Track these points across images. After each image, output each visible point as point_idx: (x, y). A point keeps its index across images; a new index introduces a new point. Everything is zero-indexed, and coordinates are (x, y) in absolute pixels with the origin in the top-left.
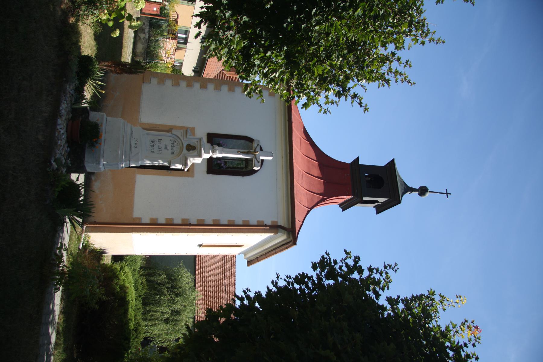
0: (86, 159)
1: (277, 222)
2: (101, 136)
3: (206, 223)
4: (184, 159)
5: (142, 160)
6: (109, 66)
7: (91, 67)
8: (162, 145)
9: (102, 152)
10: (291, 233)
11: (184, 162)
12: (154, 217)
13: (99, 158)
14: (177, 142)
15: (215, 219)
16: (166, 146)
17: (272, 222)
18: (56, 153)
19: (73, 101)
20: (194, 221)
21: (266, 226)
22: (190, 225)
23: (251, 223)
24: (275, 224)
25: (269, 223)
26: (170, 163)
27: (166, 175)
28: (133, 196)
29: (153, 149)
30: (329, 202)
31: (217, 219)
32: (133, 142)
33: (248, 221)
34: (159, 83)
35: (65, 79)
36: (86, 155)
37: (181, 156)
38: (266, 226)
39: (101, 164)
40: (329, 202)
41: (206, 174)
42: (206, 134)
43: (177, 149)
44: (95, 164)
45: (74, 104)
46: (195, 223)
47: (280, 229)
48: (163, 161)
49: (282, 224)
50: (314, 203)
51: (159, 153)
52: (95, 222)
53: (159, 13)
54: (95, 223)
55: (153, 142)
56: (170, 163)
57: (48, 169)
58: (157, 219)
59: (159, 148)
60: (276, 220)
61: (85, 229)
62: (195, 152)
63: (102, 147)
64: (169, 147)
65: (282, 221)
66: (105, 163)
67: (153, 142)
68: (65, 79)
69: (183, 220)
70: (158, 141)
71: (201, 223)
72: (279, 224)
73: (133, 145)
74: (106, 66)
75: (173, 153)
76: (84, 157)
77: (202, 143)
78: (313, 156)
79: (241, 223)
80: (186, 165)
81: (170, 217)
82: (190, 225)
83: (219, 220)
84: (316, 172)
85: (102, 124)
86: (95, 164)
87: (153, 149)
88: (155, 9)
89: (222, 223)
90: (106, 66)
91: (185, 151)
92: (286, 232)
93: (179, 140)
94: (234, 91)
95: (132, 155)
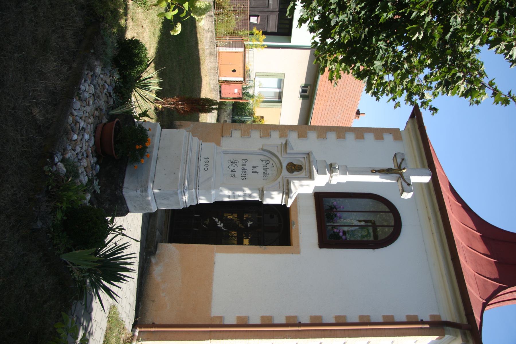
0: (126, 185)
1: (439, 316)
2: (151, 152)
3: (325, 321)
4: (285, 183)
5: (217, 188)
6: (174, 104)
7: (137, 51)
8: (249, 167)
9: (151, 174)
10: (468, 332)
11: (285, 188)
12: (243, 314)
13: (147, 182)
14: (271, 162)
15: (338, 314)
16: (254, 170)
17: (431, 316)
18: (65, 150)
19: (111, 103)
20: (305, 320)
21: (422, 322)
22: (300, 325)
23: (397, 319)
24: (436, 319)
25: (427, 319)
26: (262, 195)
27: (259, 253)
28: (211, 284)
29: (233, 174)
30: (508, 297)
31: (342, 314)
32: (202, 163)
33: (392, 317)
34: (242, 136)
35: (92, 51)
36: (126, 180)
37: (280, 179)
38: (422, 322)
39: (150, 191)
40: (508, 297)
41: (319, 249)
42: (315, 179)
43: (272, 172)
44: (139, 192)
45: (113, 108)
46: (308, 321)
47: (448, 328)
48: (250, 189)
49: (449, 319)
50: (490, 294)
51: (244, 178)
52: (153, 323)
53: (240, 96)
54: (153, 325)
55: (234, 163)
56: (262, 195)
57: (46, 168)
58: (247, 318)
59: (244, 170)
60: (436, 313)
61: (137, 334)
62: (303, 173)
63: (152, 168)
64: (260, 170)
65: (448, 314)
66: (156, 191)
67: (234, 163)
68: (92, 51)
69: (288, 318)
70: (241, 161)
71: (317, 322)
72: (444, 319)
73: (202, 167)
74: (171, 104)
75: (266, 177)
76: (123, 182)
77: (311, 159)
78: (472, 225)
79: (381, 320)
80: (287, 192)
81: (268, 315)
82: (300, 325)
83: (344, 317)
84: (481, 246)
85: (153, 136)
86: (139, 192)
87: (233, 174)
88: (236, 91)
89: (349, 321)
90: (171, 104)
91: (285, 173)
92: (458, 331)
93: (275, 159)
94: (344, 138)
95: (201, 180)
